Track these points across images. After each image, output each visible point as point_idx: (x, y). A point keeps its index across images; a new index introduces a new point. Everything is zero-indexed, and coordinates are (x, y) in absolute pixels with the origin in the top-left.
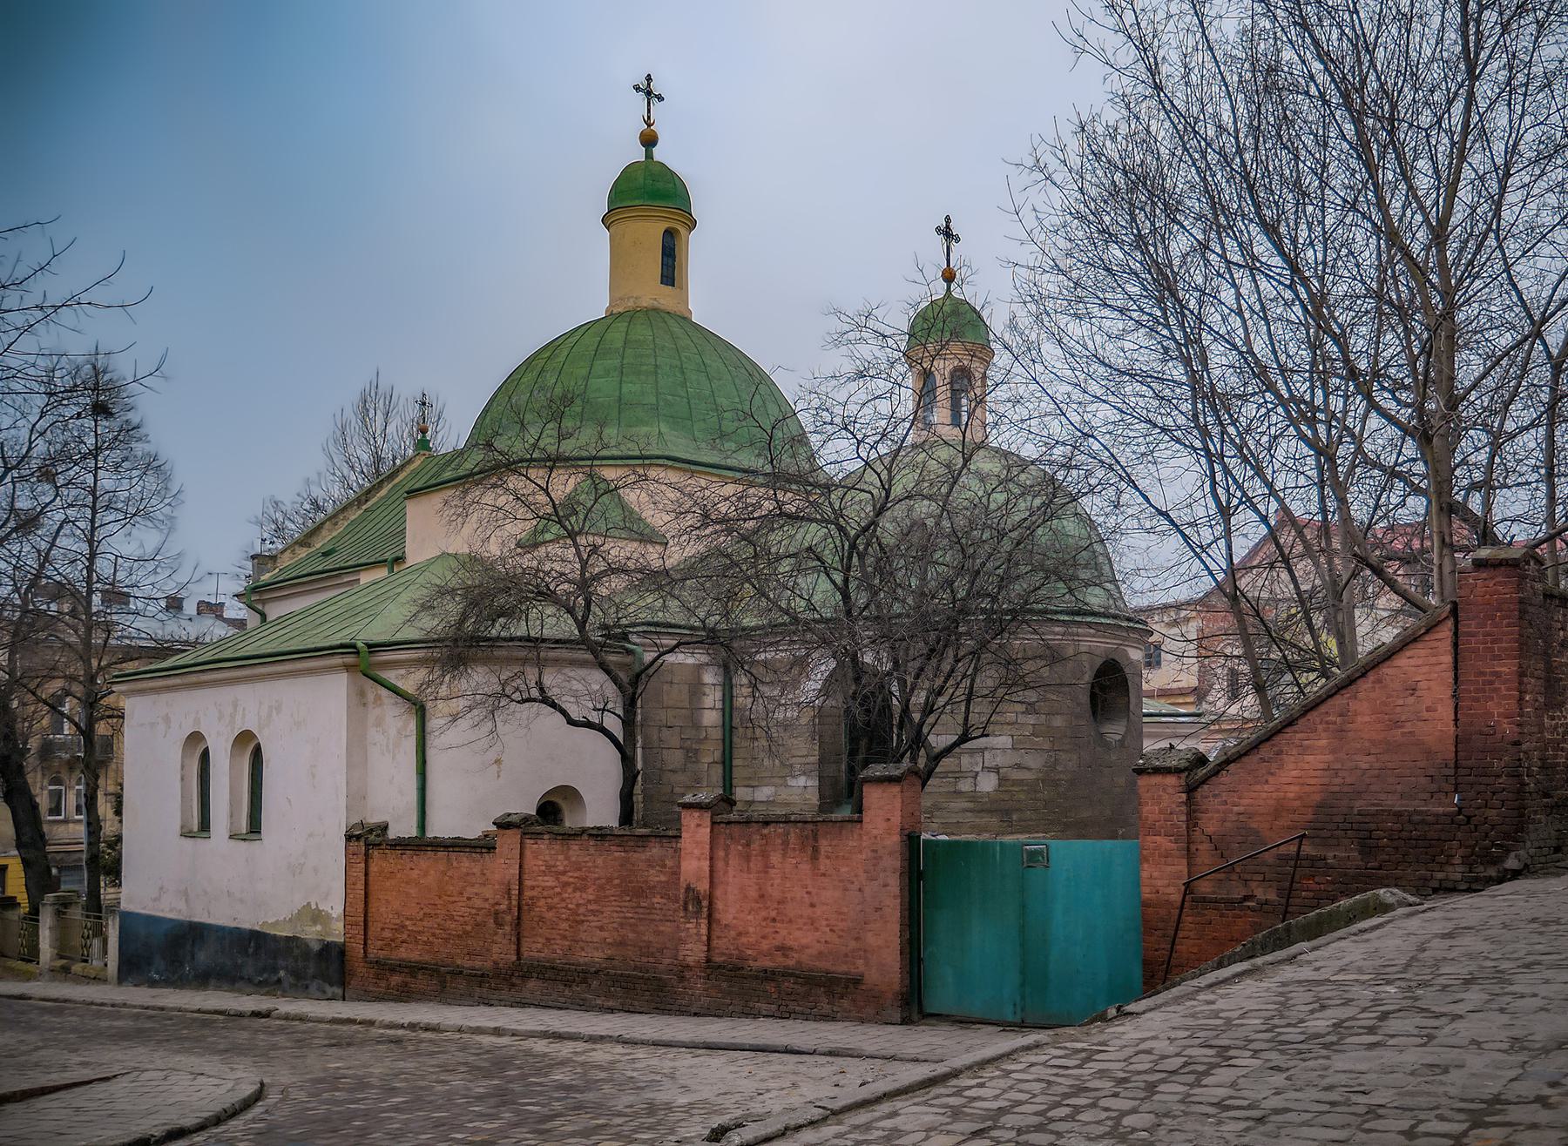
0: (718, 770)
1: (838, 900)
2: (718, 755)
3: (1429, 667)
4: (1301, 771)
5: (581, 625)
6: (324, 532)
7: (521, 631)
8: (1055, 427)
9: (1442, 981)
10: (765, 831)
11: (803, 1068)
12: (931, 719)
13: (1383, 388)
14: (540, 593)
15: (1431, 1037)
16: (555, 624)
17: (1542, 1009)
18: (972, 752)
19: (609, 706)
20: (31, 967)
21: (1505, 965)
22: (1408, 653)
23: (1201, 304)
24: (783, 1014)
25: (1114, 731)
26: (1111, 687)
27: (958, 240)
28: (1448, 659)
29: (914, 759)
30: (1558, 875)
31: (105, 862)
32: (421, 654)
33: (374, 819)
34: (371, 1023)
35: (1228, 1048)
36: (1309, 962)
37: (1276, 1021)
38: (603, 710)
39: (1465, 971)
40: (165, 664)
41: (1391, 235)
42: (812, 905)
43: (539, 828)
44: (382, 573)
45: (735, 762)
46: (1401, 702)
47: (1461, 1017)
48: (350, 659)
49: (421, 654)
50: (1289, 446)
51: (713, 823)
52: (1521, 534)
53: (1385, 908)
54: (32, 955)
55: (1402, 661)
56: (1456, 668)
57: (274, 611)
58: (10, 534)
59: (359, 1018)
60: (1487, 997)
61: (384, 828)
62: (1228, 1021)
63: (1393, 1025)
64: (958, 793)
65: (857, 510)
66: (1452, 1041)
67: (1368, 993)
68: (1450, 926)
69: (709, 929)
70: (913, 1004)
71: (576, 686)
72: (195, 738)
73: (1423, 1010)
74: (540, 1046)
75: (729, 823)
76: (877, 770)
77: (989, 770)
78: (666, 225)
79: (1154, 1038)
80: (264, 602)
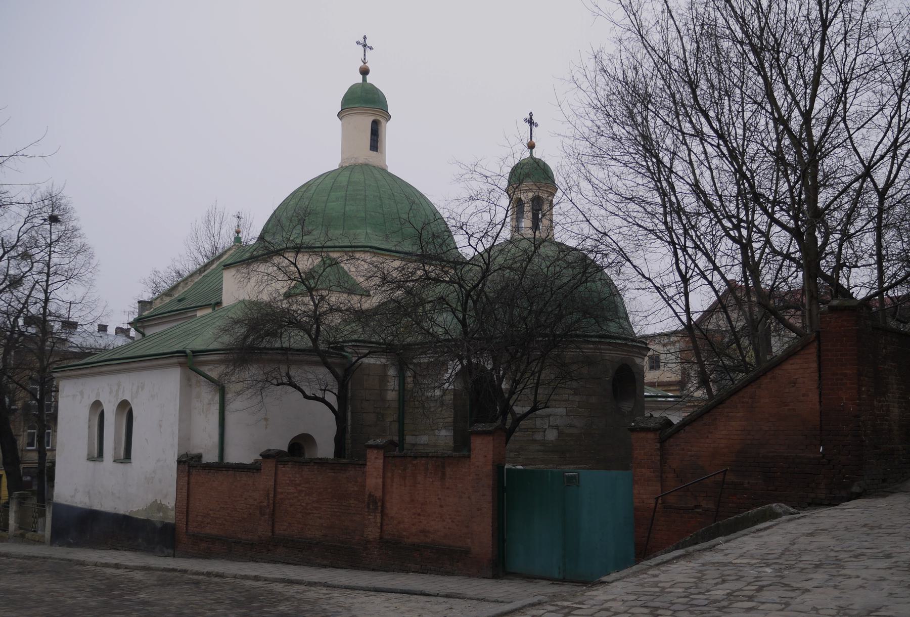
0: (395, 426)
1: (458, 505)
2: (395, 417)
3: (803, 371)
4: (728, 431)
5: (315, 341)
6: (180, 288)
7: (277, 345)
8: (586, 229)
9: (801, 565)
10: (415, 462)
11: (429, 605)
12: (515, 397)
13: (782, 210)
14: (290, 322)
15: (787, 604)
16: (298, 339)
17: (861, 587)
18: (542, 417)
19: (329, 387)
20: (4, 534)
21: (842, 556)
22: (791, 362)
23: (672, 160)
24: (423, 571)
25: (627, 406)
26: (626, 380)
27: (537, 125)
28: (814, 365)
29: (505, 419)
30: (884, 496)
31: (46, 473)
32: (222, 357)
33: (195, 451)
34: (185, 571)
35: (658, 608)
36: (722, 550)
37: (692, 591)
38: (325, 390)
39: (817, 559)
40: (91, 362)
41: (781, 121)
42: (441, 506)
43: (286, 458)
44: (209, 311)
45: (406, 421)
46: (787, 391)
47: (808, 591)
48: (182, 360)
49: (222, 357)
50: (726, 244)
51: (385, 457)
52: (860, 294)
53: (775, 515)
54: (5, 528)
55: (788, 366)
56: (820, 371)
57: (149, 332)
58: (4, 288)
59: (179, 568)
60: (827, 577)
61: (200, 457)
62: (663, 588)
63: (766, 595)
64: (534, 441)
65: (472, 275)
66: (800, 607)
67: (753, 573)
68: (813, 528)
69: (382, 519)
70: (499, 567)
71: (311, 376)
72: (97, 404)
73: (786, 585)
74: (278, 587)
75: (394, 457)
76: (480, 427)
77: (553, 427)
78: (371, 118)
79: (614, 600)
80: (144, 327)
